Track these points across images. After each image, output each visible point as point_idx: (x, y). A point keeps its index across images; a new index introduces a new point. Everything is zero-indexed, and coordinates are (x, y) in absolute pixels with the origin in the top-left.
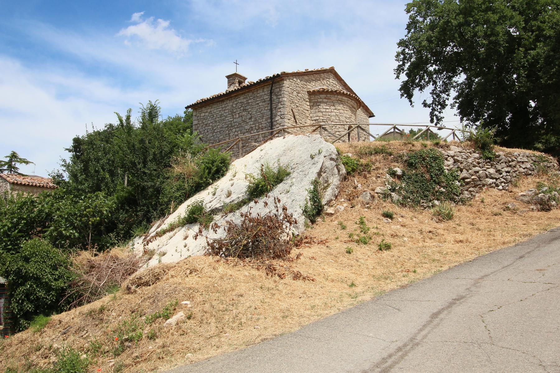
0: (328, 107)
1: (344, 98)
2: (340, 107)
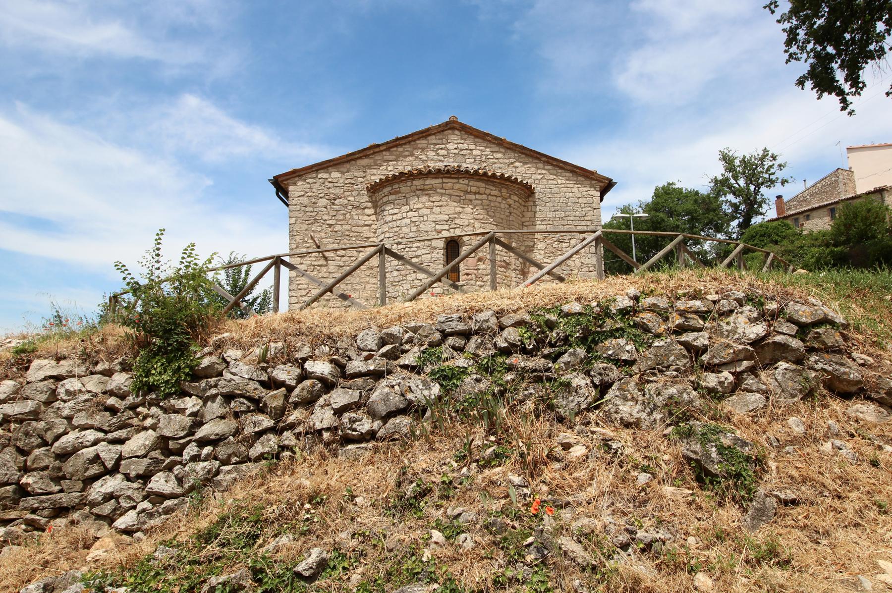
0: (396, 211)
1: (428, 182)
2: (415, 203)
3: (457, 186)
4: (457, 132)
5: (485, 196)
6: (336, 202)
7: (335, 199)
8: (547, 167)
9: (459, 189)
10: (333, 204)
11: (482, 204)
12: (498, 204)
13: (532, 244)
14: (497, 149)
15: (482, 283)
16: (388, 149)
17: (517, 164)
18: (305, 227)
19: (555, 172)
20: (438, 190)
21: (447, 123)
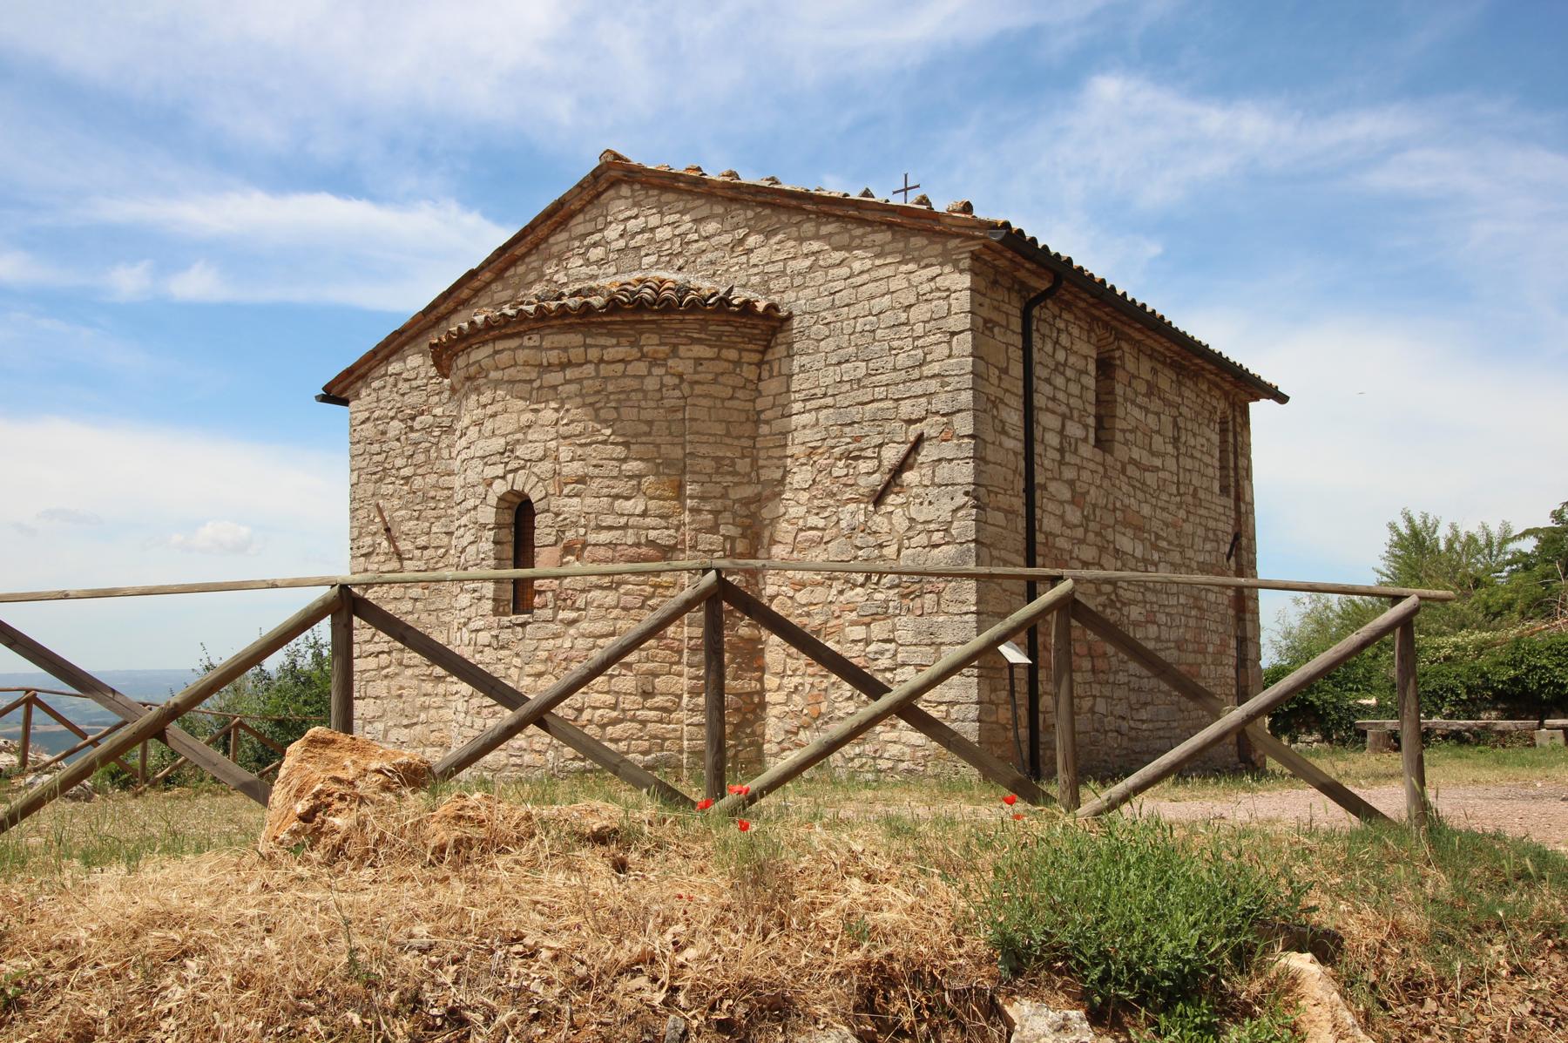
3: (522, 356)
4: (625, 190)
5: (589, 369)
6: (416, 425)
7: (413, 418)
8: (825, 230)
9: (526, 364)
10: (412, 429)
11: (582, 396)
12: (634, 384)
13: (778, 475)
14: (705, 211)
15: (574, 615)
16: (499, 275)
18: (371, 487)
19: (845, 238)
20: (493, 375)
21: (596, 175)
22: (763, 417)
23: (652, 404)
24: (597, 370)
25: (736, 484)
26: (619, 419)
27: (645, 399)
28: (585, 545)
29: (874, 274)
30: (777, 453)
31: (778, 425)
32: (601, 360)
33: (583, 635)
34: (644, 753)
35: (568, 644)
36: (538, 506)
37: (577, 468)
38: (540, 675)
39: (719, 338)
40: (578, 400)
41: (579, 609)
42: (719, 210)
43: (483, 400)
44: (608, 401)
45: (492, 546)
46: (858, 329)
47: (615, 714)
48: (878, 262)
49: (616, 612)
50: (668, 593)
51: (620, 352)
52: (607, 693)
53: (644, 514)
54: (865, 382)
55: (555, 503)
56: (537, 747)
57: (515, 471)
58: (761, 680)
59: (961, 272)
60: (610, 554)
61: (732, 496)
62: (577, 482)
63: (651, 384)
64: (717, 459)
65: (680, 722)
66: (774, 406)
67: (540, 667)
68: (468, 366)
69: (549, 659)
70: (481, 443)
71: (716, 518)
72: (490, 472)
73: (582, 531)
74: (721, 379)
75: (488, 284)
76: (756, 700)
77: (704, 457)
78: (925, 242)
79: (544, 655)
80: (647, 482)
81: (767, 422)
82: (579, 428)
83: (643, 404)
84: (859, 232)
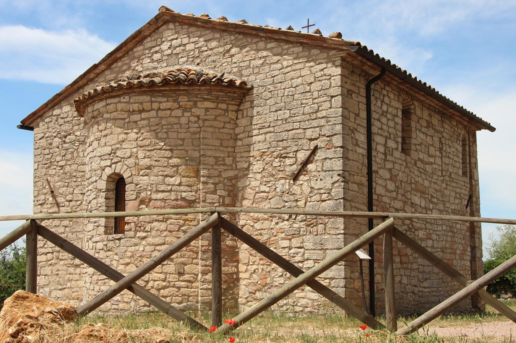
3: (120, 106)
4: (171, 26)
5: (153, 113)
6: (67, 140)
7: (65, 137)
8: (269, 46)
9: (122, 110)
11: (149, 125)
12: (175, 120)
13: (246, 165)
14: (210, 36)
15: (145, 234)
16: (109, 67)
17: (234, 51)
18: (44, 171)
19: (279, 50)
22: (239, 137)
23: (184, 130)
24: (157, 114)
25: (225, 170)
26: (168, 138)
27: (181, 128)
28: (150, 200)
29: (294, 67)
30: (245, 155)
31: (246, 141)
32: (159, 109)
33: (149, 245)
34: (179, 303)
35: (141, 249)
36: (127, 181)
37: (147, 162)
38: (127, 264)
39: (217, 98)
40: (148, 128)
41: (147, 232)
42: (217, 35)
43: (101, 128)
44: (162, 129)
45: (104, 200)
46: (286, 94)
47: (164, 284)
48: (295, 62)
49: (165, 233)
50: (191, 224)
51: (169, 105)
52: (161, 273)
53: (180, 185)
54: (289, 120)
55: (136, 179)
56: (126, 300)
57: (116, 163)
58: (237, 267)
59: (336, 66)
60: (163, 204)
61: (223, 176)
62: (147, 169)
63: (184, 120)
64: (216, 158)
65: (197, 287)
66: (244, 131)
67: (128, 260)
68: (93, 111)
69: (132, 256)
70: (99, 149)
71: (215, 187)
72: (104, 163)
73: (149, 193)
74: (218, 118)
75: (103, 71)
76: (235, 277)
77: (209, 157)
78: (319, 52)
79: (129, 254)
80: (181, 169)
81: (241, 140)
82: (147, 142)
83: (180, 130)
84: (286, 47)
